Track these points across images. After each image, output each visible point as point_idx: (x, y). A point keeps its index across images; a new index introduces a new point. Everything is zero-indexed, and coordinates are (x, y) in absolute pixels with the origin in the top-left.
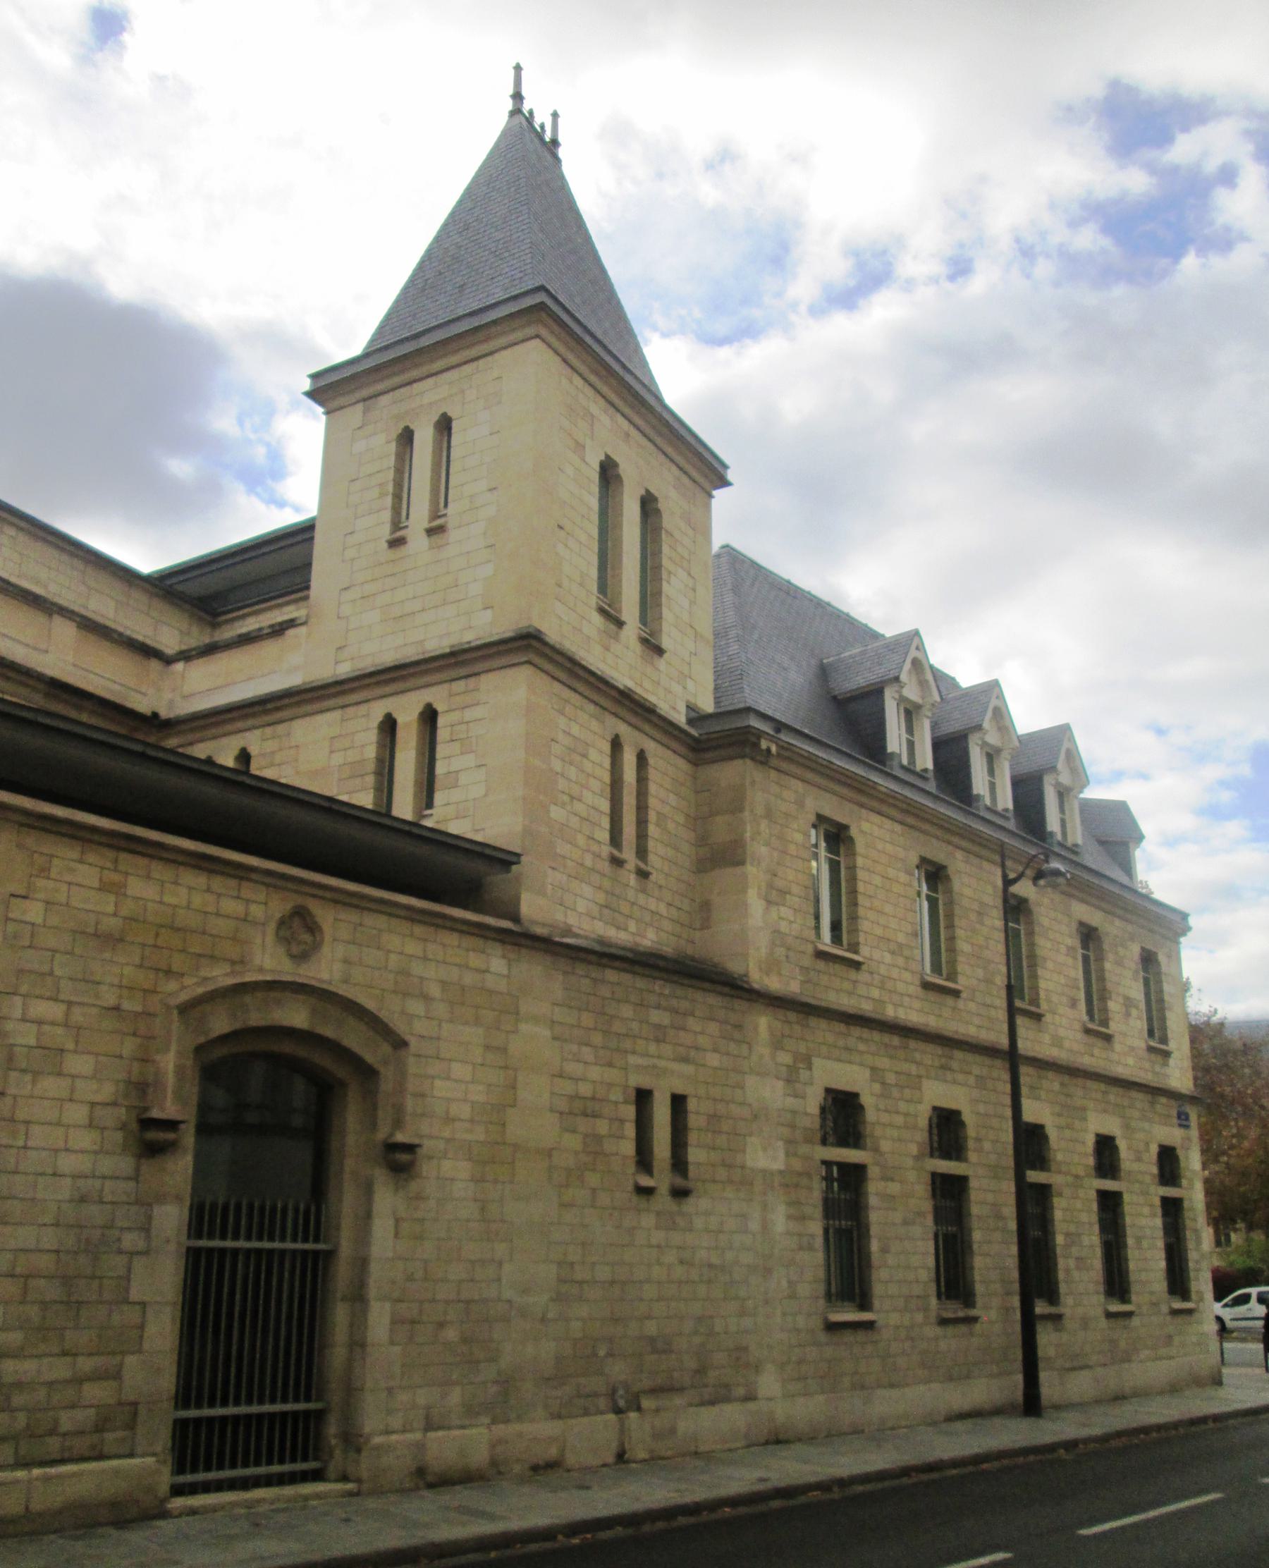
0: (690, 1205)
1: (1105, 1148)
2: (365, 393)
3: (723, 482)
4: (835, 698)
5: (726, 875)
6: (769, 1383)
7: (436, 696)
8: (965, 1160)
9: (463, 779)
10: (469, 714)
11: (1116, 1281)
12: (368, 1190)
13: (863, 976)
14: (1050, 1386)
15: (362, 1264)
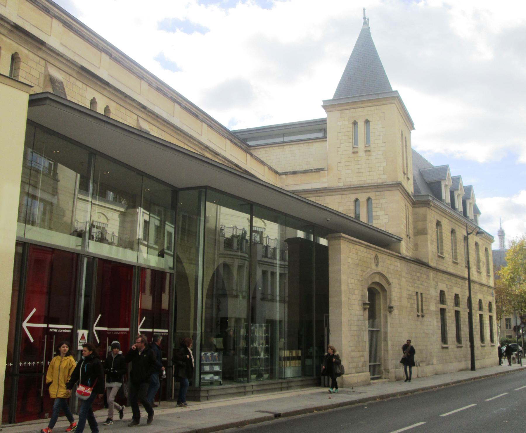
0: (425, 318)
2: (341, 108)
3: (414, 129)
4: (426, 183)
5: (422, 237)
6: (435, 361)
7: (371, 195)
8: (459, 307)
9: (381, 217)
10: (382, 201)
11: (482, 339)
12: (386, 317)
13: (444, 261)
14: (477, 364)
15: (386, 333)
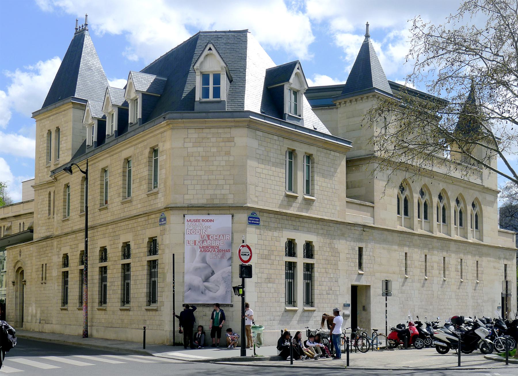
1: (104, 250)
